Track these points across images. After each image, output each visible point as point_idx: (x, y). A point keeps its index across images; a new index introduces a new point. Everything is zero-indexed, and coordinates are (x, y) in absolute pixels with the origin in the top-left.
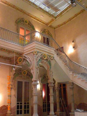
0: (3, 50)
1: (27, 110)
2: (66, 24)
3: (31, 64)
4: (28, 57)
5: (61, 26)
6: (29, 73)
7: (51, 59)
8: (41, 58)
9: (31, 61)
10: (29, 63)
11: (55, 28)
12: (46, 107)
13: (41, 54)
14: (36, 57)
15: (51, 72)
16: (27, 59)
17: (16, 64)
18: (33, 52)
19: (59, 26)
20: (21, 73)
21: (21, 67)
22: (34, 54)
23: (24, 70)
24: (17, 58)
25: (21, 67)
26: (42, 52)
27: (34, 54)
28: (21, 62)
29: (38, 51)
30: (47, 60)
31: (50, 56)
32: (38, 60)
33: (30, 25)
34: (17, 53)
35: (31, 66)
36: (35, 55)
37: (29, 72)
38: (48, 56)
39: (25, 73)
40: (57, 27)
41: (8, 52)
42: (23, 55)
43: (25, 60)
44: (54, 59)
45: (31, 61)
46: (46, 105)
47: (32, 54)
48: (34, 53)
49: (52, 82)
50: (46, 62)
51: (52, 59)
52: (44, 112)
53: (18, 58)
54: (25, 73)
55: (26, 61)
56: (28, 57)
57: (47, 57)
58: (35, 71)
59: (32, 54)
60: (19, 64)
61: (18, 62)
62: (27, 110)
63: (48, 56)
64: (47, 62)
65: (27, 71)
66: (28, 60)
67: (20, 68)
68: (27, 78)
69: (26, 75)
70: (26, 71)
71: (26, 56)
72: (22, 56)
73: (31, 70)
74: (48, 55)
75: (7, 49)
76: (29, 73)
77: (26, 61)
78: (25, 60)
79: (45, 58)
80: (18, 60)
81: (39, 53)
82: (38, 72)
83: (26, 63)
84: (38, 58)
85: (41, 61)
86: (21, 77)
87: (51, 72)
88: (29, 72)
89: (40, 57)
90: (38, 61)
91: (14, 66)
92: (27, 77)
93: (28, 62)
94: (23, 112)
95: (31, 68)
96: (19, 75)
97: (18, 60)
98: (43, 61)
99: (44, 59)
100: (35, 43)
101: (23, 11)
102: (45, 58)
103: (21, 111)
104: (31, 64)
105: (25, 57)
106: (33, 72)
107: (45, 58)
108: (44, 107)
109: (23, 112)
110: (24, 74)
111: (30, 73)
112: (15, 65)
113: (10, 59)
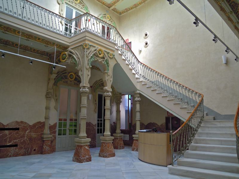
0: (37, 39)
1: (64, 121)
2: (138, 7)
3: (79, 63)
4: (75, 52)
5: (130, 11)
6: (78, 77)
7: (109, 56)
8: (94, 54)
9: (79, 58)
10: (76, 61)
11: (120, 13)
12: (101, 127)
13: (94, 49)
14: (88, 53)
15: (109, 76)
16: (74, 56)
17: (58, 62)
18: (83, 46)
19: (127, 10)
20: (66, 77)
21: (65, 67)
22: (84, 48)
23: (70, 72)
24: (59, 53)
25: (65, 67)
26: (97, 46)
27: (84, 48)
28: (65, 60)
29: (91, 44)
30: (103, 58)
31: (108, 53)
32: (90, 57)
33: (84, 5)
34: (60, 46)
35: (79, 65)
36: (86, 49)
37: (78, 76)
38: (106, 53)
39: (72, 77)
40: (124, 11)
41: (46, 44)
42: (68, 49)
43: (71, 57)
44: (115, 58)
45: (79, 58)
46: (101, 123)
47: (81, 47)
48: (85, 47)
49: (109, 90)
50: (102, 61)
51: (112, 57)
52: (98, 133)
53: (61, 53)
54: (72, 77)
55: (72, 58)
56: (75, 52)
57: (104, 53)
58: (85, 72)
59: (81, 47)
60: (63, 62)
61: (61, 60)
62: (64, 121)
63: (106, 53)
64: (104, 61)
65: (75, 74)
66: (75, 57)
67: (65, 70)
68: (75, 84)
69: (73, 79)
70: (74, 74)
71: (72, 51)
72: (66, 51)
73: (78, 71)
74: (105, 51)
75: (43, 38)
76: (78, 77)
77: (72, 58)
78: (71, 57)
79: (100, 56)
80: (61, 57)
81: (92, 47)
82: (88, 75)
83: (72, 62)
84: (90, 54)
85: (94, 58)
86: (67, 82)
87: (109, 76)
88: (78, 76)
89: (93, 53)
90: (90, 59)
91: (55, 64)
92: (75, 83)
93: (75, 59)
94: (68, 132)
95: (78, 68)
96: (64, 79)
97: (61, 57)
98: (98, 59)
99: (98, 56)
100: (86, 32)
101: (128, 9)
102: (100, 56)
103: (65, 130)
104: (79, 63)
105: (70, 52)
106: (82, 75)
107: (100, 55)
108: (98, 127)
109: (68, 132)
110: (72, 79)
111: (79, 77)
112: (57, 63)
113: (50, 56)
